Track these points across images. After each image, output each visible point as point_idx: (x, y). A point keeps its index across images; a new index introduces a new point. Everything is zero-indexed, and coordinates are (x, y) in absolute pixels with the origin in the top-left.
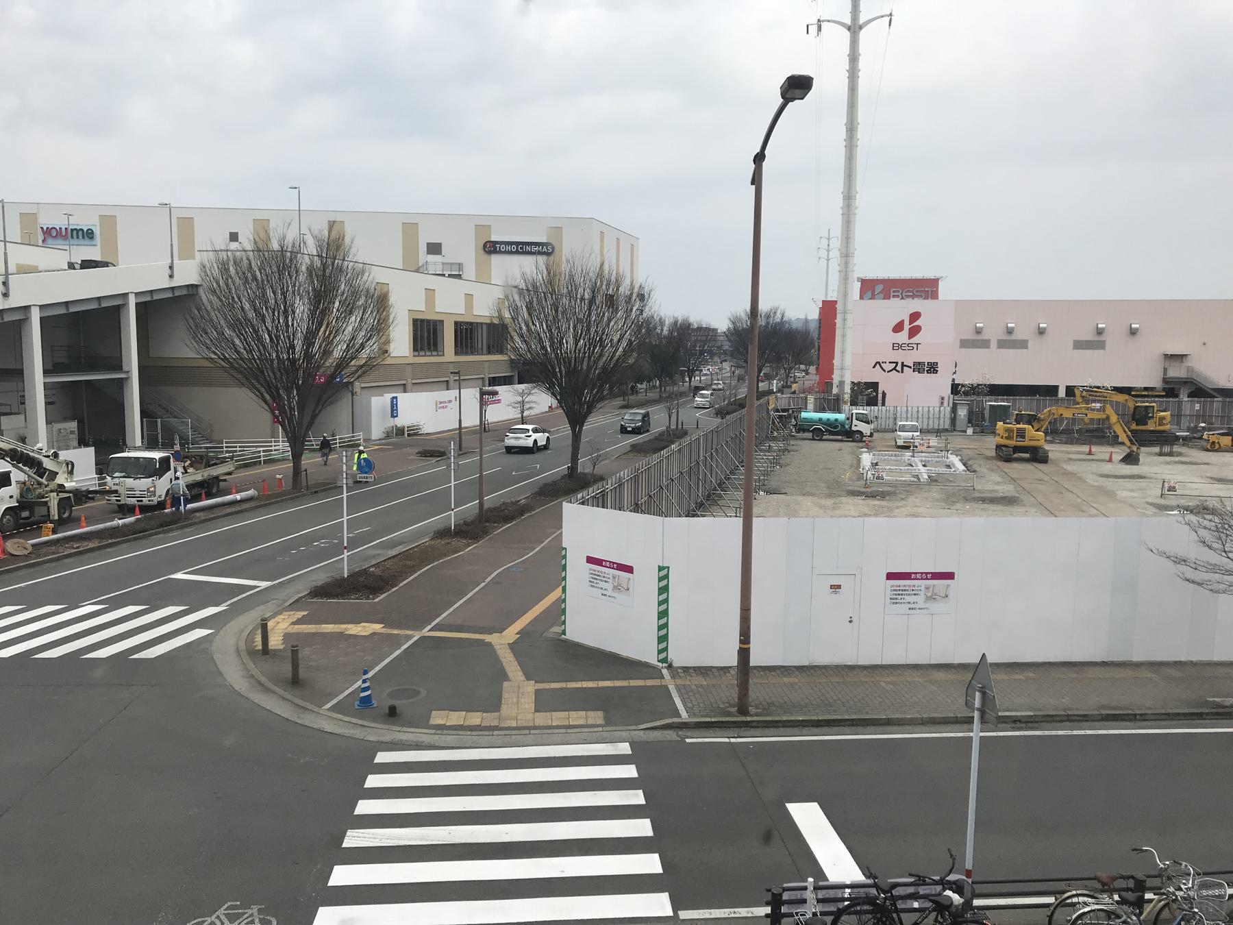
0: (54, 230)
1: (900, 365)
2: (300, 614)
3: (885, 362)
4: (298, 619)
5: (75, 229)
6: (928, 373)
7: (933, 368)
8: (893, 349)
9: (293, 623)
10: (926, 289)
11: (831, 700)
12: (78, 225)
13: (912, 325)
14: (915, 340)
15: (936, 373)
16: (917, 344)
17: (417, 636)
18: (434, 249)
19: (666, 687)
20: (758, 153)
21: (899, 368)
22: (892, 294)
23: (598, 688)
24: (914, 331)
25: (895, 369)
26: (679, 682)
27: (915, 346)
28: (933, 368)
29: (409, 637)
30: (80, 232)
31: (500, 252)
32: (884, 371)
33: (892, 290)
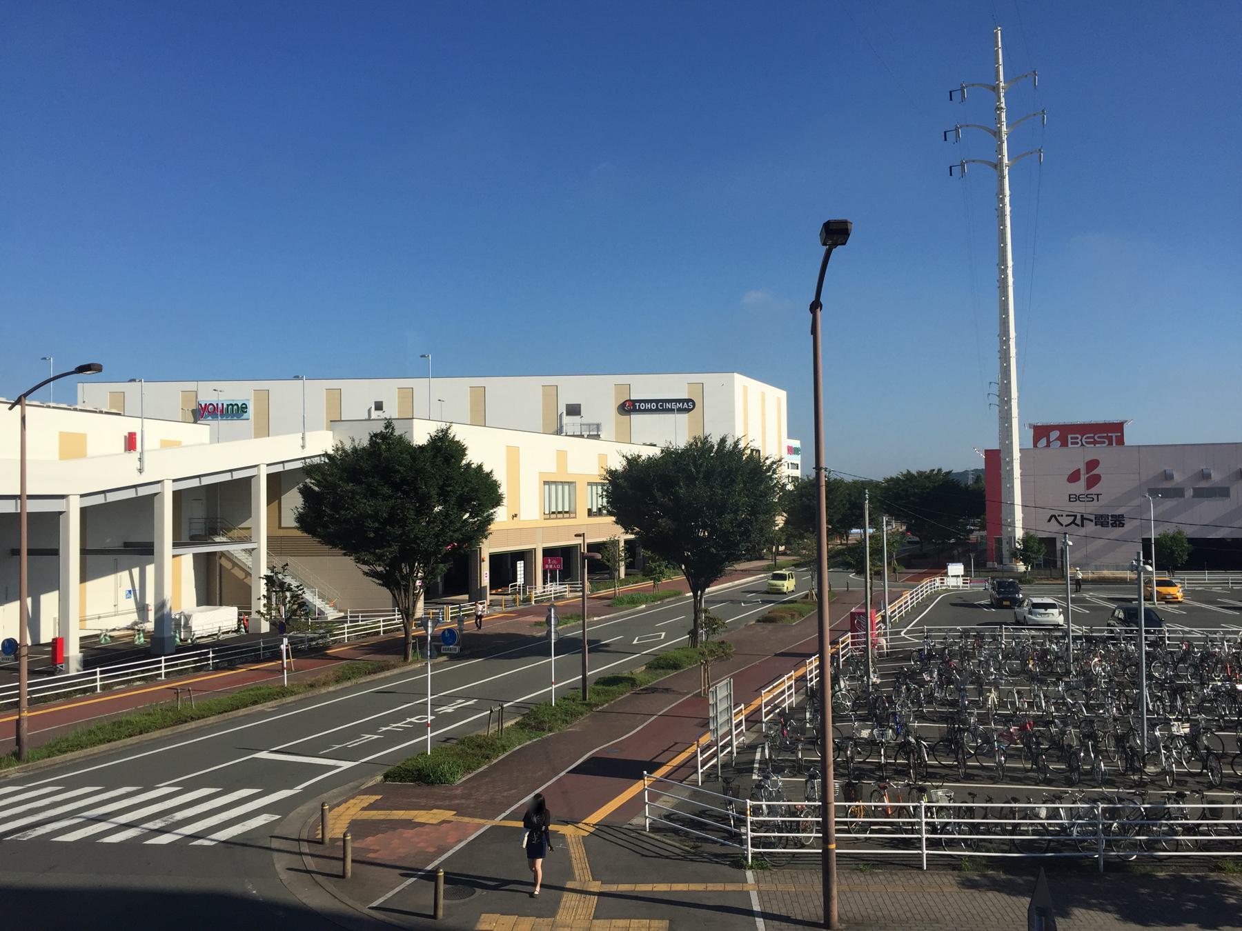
0: (211, 406)
1: (1079, 517)
2: (373, 798)
3: (1062, 516)
4: (371, 804)
5: (231, 404)
6: (1112, 526)
7: (1118, 521)
8: (1070, 501)
9: (364, 809)
10: (1109, 434)
11: (939, 915)
12: (233, 400)
13: (1089, 475)
14: (1093, 490)
15: (1123, 526)
16: (1098, 495)
17: (489, 824)
18: (574, 410)
19: (748, 893)
20: (813, 302)
21: (1078, 521)
22: (1070, 441)
23: (689, 891)
24: (1093, 481)
25: (1073, 522)
26: (764, 887)
27: (1095, 497)
28: (1119, 521)
29: (480, 826)
30: (235, 407)
31: (640, 411)
32: (1062, 525)
33: (1069, 436)
